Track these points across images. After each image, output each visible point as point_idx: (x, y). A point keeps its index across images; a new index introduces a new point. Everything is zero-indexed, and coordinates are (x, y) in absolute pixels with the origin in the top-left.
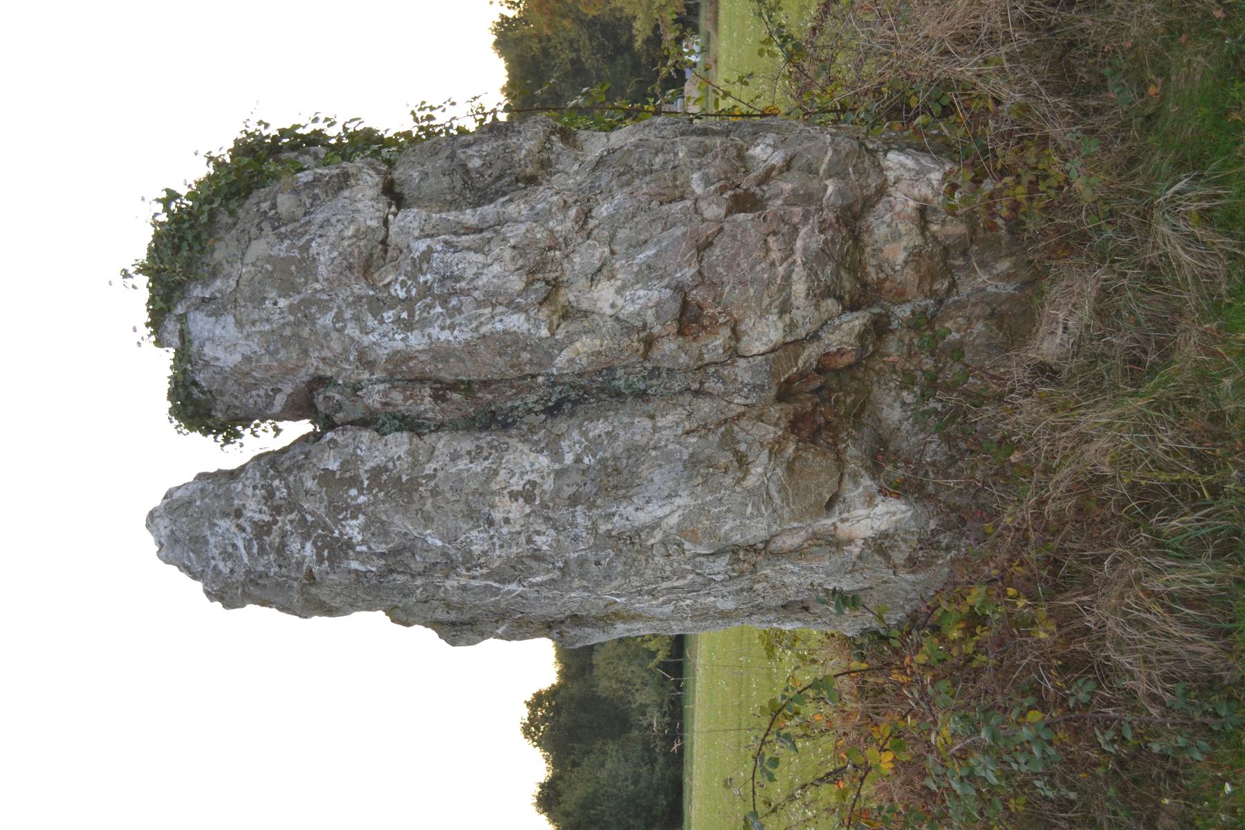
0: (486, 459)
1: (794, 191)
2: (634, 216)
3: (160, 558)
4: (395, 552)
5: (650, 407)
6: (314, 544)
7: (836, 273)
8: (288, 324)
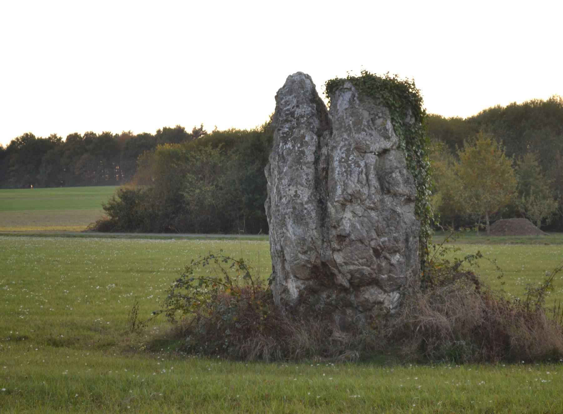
0: (306, 183)
1: (382, 266)
2: (371, 222)
3: (288, 77)
4: (283, 157)
5: (319, 228)
6: (288, 131)
7: (358, 278)
8: (345, 124)
